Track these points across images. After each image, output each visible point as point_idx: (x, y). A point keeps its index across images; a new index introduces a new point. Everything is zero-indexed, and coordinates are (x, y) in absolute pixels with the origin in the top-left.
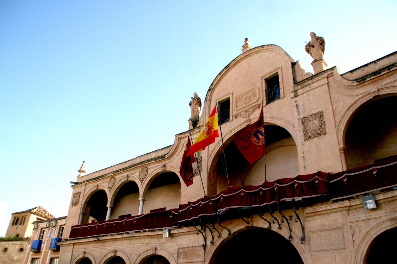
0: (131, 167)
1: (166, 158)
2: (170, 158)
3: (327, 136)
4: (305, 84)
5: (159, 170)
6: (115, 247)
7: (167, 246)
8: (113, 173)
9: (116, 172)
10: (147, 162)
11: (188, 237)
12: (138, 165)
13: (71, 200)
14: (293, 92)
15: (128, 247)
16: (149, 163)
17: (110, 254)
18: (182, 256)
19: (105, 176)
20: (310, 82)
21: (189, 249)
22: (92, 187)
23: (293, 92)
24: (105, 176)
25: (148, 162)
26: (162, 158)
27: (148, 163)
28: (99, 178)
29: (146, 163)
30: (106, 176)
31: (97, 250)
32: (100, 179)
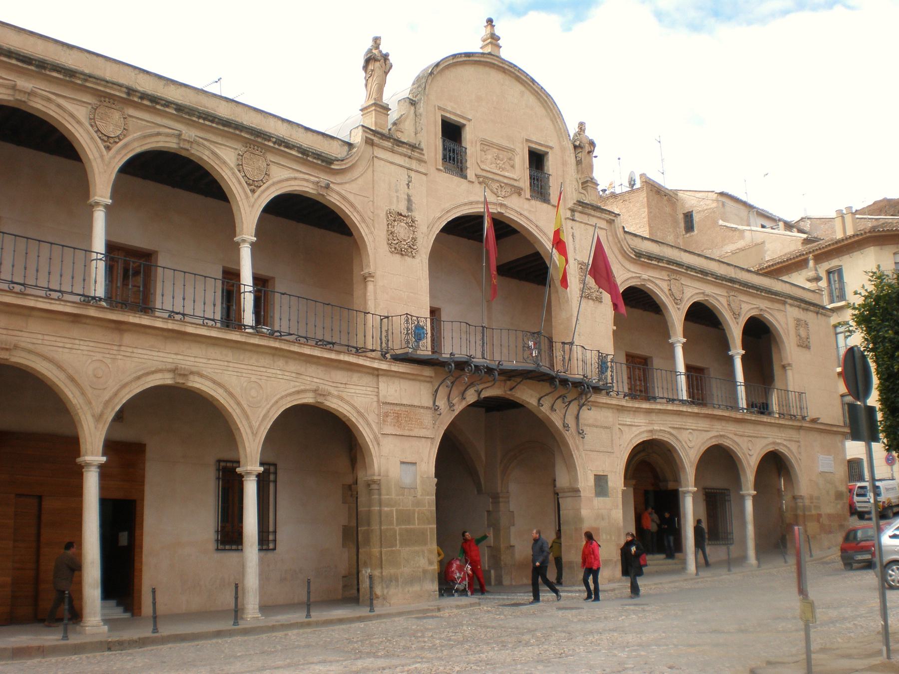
0: (212, 121)
1: (333, 167)
2: (627, 259)
3: (603, 305)
4: (587, 211)
5: (305, 184)
6: (179, 357)
7: (353, 391)
8: (128, 94)
9: (142, 98)
10: (275, 143)
11: (797, 630)
12: (241, 131)
13: (141, 579)
14: (570, 209)
15: (230, 369)
16: (282, 148)
17: (159, 376)
18: (389, 419)
19: (79, 78)
20: (592, 212)
21: (403, 408)
22: (634, 275)
23: (570, 209)
24: (82, 77)
25: (280, 145)
26: (323, 161)
27: (276, 146)
28: (45, 68)
29: (271, 144)
30: (86, 80)
31: (82, 347)
32: (48, 73)
